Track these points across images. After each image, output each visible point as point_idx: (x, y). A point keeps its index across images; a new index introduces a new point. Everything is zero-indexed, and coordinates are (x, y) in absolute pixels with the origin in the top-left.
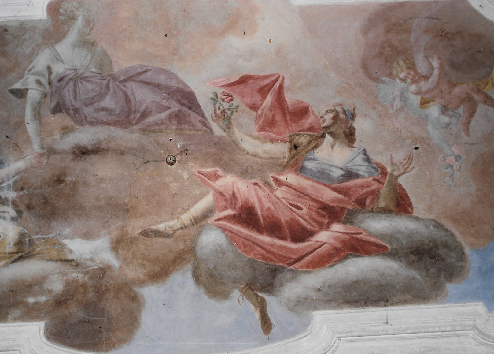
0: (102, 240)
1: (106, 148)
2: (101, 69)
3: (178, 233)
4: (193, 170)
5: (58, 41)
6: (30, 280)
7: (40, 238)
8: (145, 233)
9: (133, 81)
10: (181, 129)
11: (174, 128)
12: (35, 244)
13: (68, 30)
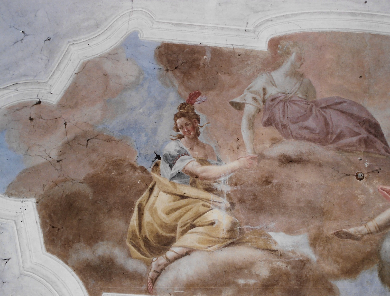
0: (302, 236)
1: (307, 159)
2: (307, 96)
3: (365, 237)
4: (377, 186)
5: (274, 69)
6: (240, 264)
7: (249, 228)
8: (338, 234)
9: (331, 108)
10: (368, 152)
11: (363, 150)
12: (245, 233)
13: (283, 63)
